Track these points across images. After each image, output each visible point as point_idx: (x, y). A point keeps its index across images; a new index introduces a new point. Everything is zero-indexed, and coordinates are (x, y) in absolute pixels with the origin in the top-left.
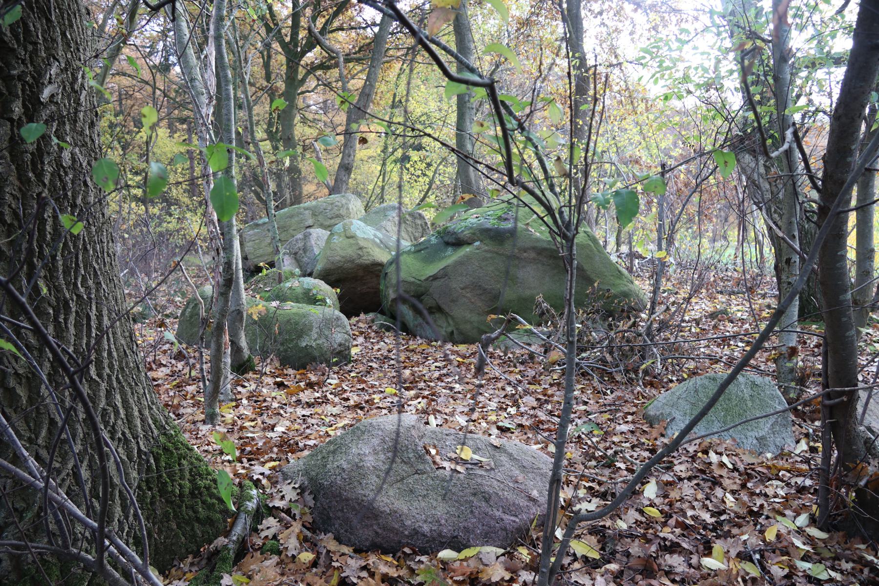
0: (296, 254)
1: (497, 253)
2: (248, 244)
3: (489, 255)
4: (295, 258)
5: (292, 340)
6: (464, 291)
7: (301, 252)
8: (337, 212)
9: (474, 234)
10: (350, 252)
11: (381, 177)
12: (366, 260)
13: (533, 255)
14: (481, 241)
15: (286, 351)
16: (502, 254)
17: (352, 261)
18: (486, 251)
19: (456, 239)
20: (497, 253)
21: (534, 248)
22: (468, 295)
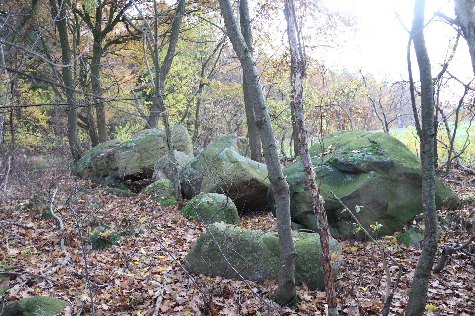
0: (164, 168)
1: (385, 178)
2: (121, 161)
3: (381, 180)
4: (164, 172)
5: (315, 268)
6: (368, 206)
7: (168, 167)
8: (180, 138)
9: (368, 166)
10: (239, 173)
11: (466, 146)
12: (248, 178)
13: (404, 178)
14: (375, 171)
15: (311, 277)
16: (388, 179)
17: (240, 179)
18: (379, 177)
19: (353, 169)
20: (385, 178)
21: (405, 174)
22: (370, 208)
